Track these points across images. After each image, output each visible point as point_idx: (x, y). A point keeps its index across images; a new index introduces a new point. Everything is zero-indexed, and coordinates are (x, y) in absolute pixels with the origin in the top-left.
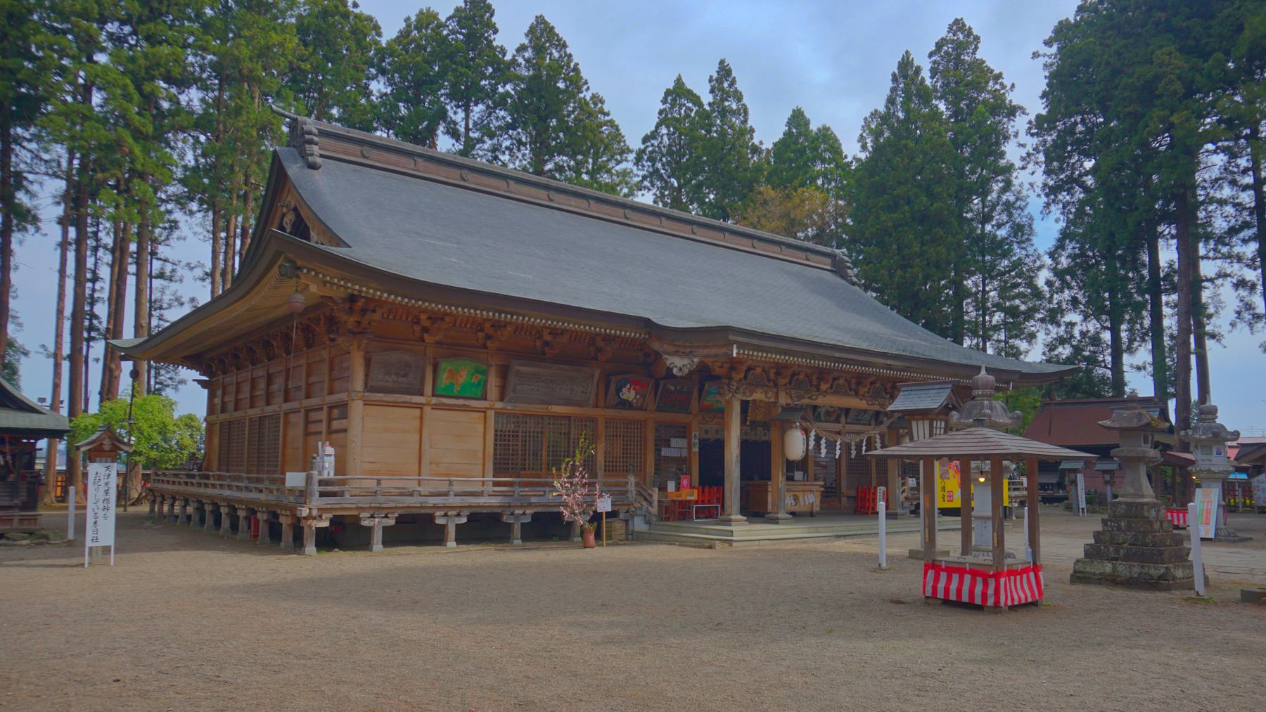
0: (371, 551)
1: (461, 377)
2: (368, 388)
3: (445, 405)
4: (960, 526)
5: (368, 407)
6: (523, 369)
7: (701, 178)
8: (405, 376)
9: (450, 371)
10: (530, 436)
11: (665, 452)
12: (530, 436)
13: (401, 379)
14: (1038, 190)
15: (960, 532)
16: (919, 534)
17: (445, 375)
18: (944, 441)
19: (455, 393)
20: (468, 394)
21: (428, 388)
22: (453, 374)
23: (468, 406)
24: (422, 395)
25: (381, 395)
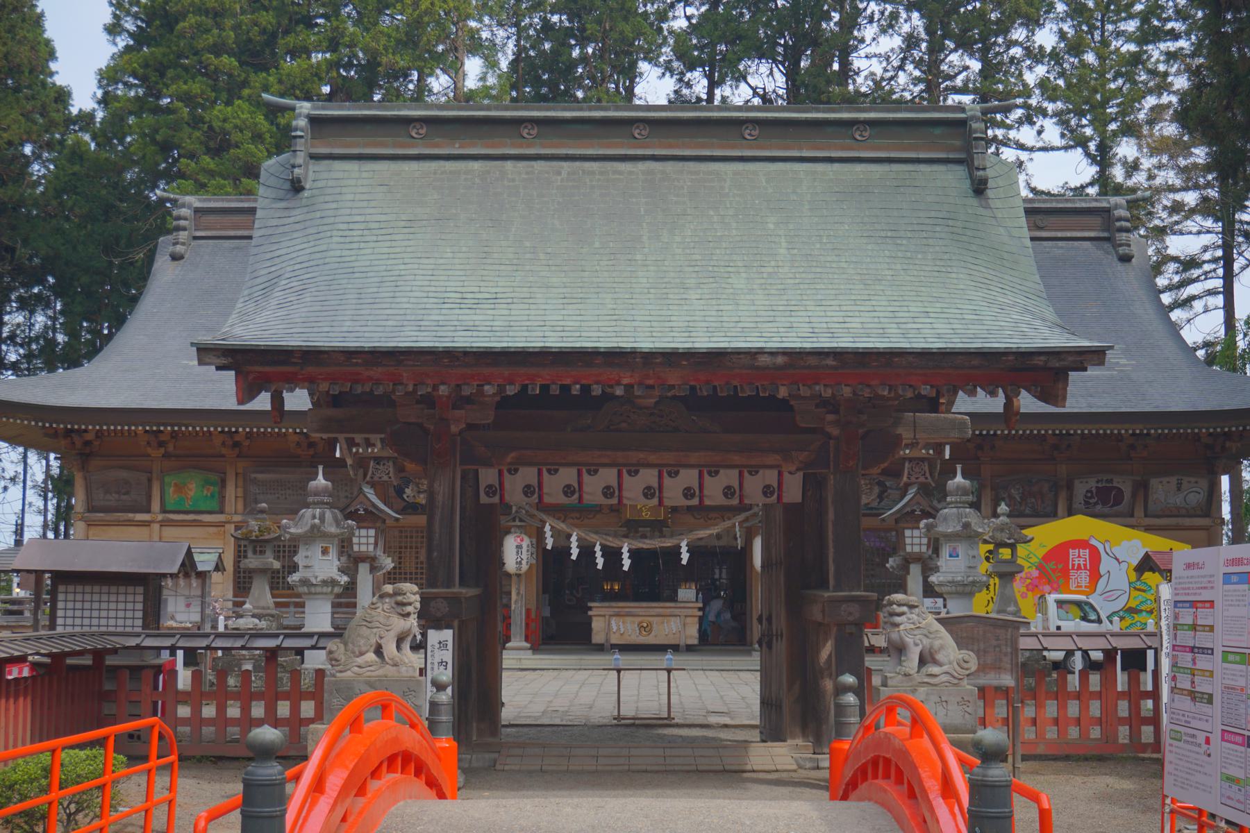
0: (925, 597)
1: (191, 490)
2: (91, 508)
3: (173, 521)
4: (759, 668)
5: (93, 527)
6: (259, 476)
7: (411, 86)
8: (127, 493)
9: (176, 485)
10: (284, 551)
11: (1226, 613)
12: (284, 551)
13: (124, 497)
14: (926, 641)
15: (759, 673)
16: (503, 723)
17: (172, 489)
18: (443, 267)
19: (188, 507)
20: (203, 508)
21: (156, 506)
22: (179, 488)
23: (200, 521)
24: (149, 511)
25: (102, 515)
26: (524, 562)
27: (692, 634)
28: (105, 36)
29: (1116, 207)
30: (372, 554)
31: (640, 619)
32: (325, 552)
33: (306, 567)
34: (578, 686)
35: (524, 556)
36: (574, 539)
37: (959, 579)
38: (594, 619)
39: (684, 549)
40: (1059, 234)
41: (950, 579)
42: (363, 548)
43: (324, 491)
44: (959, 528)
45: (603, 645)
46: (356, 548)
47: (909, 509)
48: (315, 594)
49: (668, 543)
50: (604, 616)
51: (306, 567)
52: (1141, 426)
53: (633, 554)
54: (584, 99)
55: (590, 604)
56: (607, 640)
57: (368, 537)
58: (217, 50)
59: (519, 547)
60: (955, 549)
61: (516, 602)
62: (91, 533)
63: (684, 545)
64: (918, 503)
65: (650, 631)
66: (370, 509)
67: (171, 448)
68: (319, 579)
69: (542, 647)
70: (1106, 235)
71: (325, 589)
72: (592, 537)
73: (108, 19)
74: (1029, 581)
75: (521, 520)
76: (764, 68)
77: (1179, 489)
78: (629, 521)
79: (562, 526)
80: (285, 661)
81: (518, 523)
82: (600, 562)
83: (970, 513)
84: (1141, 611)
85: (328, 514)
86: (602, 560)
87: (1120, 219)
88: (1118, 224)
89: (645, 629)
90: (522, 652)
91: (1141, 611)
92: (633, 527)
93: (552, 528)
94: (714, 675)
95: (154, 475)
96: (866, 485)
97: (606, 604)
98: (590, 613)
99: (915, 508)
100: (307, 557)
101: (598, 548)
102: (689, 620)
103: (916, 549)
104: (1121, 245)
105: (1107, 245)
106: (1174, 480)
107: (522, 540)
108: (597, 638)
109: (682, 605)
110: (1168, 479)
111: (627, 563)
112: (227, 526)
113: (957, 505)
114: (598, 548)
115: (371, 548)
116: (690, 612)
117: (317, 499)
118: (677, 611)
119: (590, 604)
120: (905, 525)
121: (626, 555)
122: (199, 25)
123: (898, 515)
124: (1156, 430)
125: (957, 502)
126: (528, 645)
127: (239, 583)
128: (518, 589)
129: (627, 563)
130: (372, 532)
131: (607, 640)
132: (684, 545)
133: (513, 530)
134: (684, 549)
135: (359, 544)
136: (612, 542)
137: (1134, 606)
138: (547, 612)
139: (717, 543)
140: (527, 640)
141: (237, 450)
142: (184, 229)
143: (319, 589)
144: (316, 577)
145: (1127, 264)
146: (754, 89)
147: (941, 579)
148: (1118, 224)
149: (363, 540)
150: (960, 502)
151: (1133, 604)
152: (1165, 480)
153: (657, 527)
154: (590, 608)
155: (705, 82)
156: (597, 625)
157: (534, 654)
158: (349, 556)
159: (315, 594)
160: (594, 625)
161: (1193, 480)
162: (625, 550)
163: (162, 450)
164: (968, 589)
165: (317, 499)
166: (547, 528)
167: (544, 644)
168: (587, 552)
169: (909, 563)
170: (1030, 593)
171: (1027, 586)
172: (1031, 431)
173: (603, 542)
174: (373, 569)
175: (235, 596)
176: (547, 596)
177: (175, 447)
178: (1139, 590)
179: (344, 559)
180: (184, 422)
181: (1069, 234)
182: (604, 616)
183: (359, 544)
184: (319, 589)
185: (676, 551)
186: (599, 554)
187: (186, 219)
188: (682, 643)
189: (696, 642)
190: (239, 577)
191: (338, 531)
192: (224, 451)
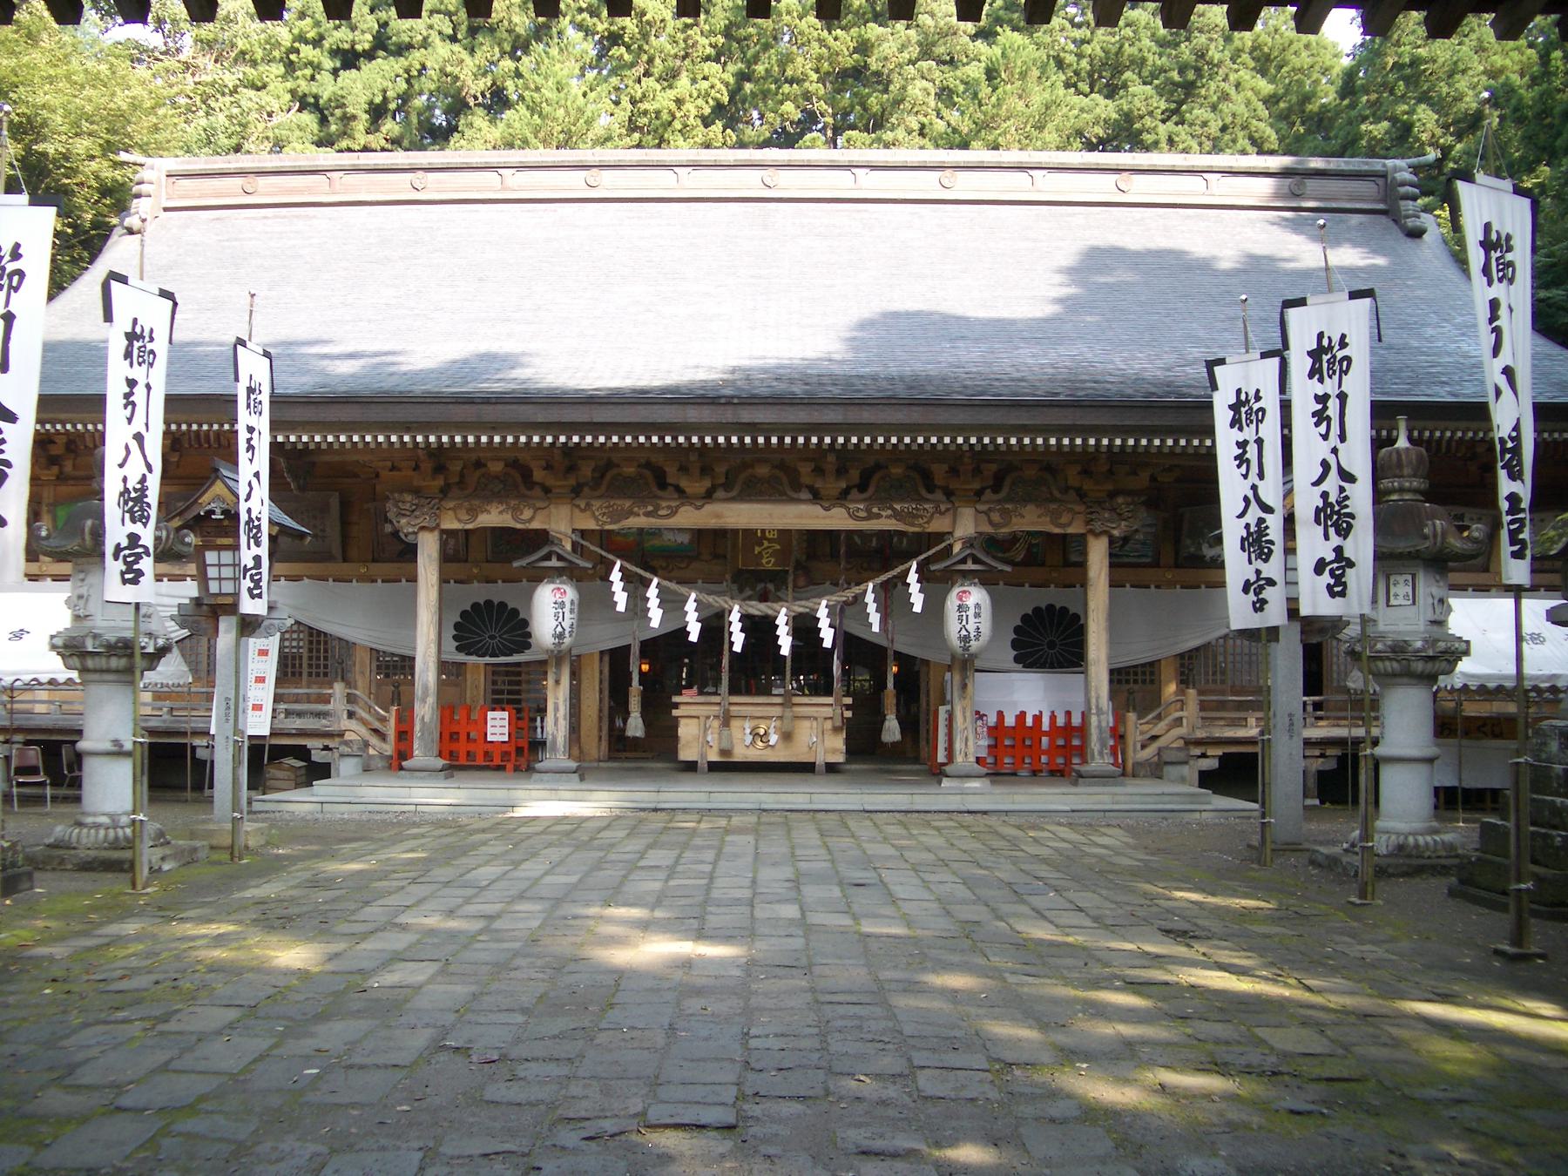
29: (1396, 169)
31: (755, 722)
38: (683, 722)
45: (695, 763)
54: (1032, 739)
55: (676, 699)
67: (68, 467)
72: (718, 602)
75: (560, 558)
79: (758, 608)
86: (743, 635)
87: (1403, 184)
95: (45, 508)
98: (675, 713)
108: (686, 754)
119: (676, 699)
127: (1136, 674)
145: (1417, 240)
146: (949, 125)
154: (676, 705)
160: (682, 731)
162: (781, 620)
163: (55, 469)
164: (1429, 667)
177: (74, 465)
189: (840, 758)
190: (1128, 673)
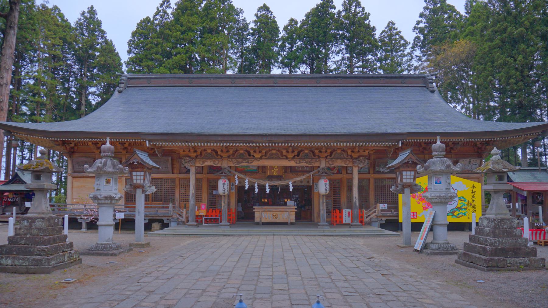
26: (226, 190)
27: (292, 218)
28: (126, 53)
30: (142, 184)
31: (273, 213)
32: (108, 182)
33: (98, 190)
34: (238, 258)
35: (226, 188)
36: (247, 181)
37: (443, 195)
39: (291, 185)
40: (409, 85)
41: (438, 195)
42: (138, 181)
43: (109, 150)
44: (443, 168)
46: (135, 181)
47: (406, 161)
48: (102, 204)
49: (284, 183)
50: (259, 211)
51: (98, 190)
52: (463, 138)
53: (271, 187)
55: (254, 207)
56: (261, 221)
57: (140, 176)
58: (157, 53)
59: (224, 184)
60: (438, 179)
61: (224, 206)
62: (74, 181)
63: (290, 183)
64: (411, 158)
65: (277, 218)
66: (140, 161)
68: (102, 196)
69: (237, 223)
70: (424, 85)
71: (106, 202)
72: (254, 180)
73: (127, 49)
74: (420, 197)
75: (225, 173)
76: (304, 66)
77: (469, 163)
78: (269, 176)
79: (242, 176)
80: (45, 248)
81: (224, 174)
82: (257, 190)
83: (447, 160)
84: (462, 208)
85: (109, 162)
88: (429, 81)
89: (275, 216)
90: (226, 227)
91: (462, 208)
92: (270, 178)
93: (238, 177)
94: (306, 239)
96: (363, 159)
97: (260, 207)
98: (254, 210)
99: (409, 160)
100: (98, 184)
101: (256, 185)
102: (291, 213)
103: (408, 181)
104: (431, 87)
105: (425, 88)
106: (468, 160)
107: (225, 181)
108: (257, 220)
109: (289, 207)
110: (465, 160)
111: (268, 191)
112: (122, 178)
113: (438, 156)
114: (256, 185)
115: (142, 181)
116: (292, 210)
117: (106, 154)
118: (287, 210)
120: (404, 169)
121: (267, 188)
122: (151, 47)
123: (401, 164)
124: (469, 139)
125: (439, 155)
126: (228, 224)
128: (323, 200)
129: (268, 191)
130: (142, 173)
131: (261, 221)
132: (290, 183)
133: (222, 177)
134: (291, 185)
135: (136, 179)
136: (262, 182)
137: (460, 206)
138: (240, 209)
139: (300, 184)
140: (229, 222)
141: (126, 151)
142: (123, 83)
143: (103, 202)
144: (101, 195)
147: (433, 195)
148: (429, 81)
149: (138, 177)
150: (441, 155)
151: (459, 206)
152: (465, 160)
153: (279, 178)
154: (254, 209)
155: (289, 71)
156: (257, 215)
157: (230, 227)
158: (131, 185)
159: (102, 204)
161: (475, 160)
164: (443, 200)
165: (106, 154)
166: (236, 177)
167: (238, 221)
168: (252, 188)
169: (404, 188)
170: (421, 202)
171: (420, 199)
172: (422, 140)
173: (258, 182)
174: (143, 192)
175: (125, 204)
176: (240, 204)
178: (461, 200)
179: (128, 187)
180: (100, 137)
181: (412, 85)
182: (259, 211)
183: (136, 179)
184: (103, 202)
185: (288, 186)
186: (256, 187)
187: (124, 80)
188: (289, 222)
189: (294, 221)
191: (113, 170)
192: (121, 151)
